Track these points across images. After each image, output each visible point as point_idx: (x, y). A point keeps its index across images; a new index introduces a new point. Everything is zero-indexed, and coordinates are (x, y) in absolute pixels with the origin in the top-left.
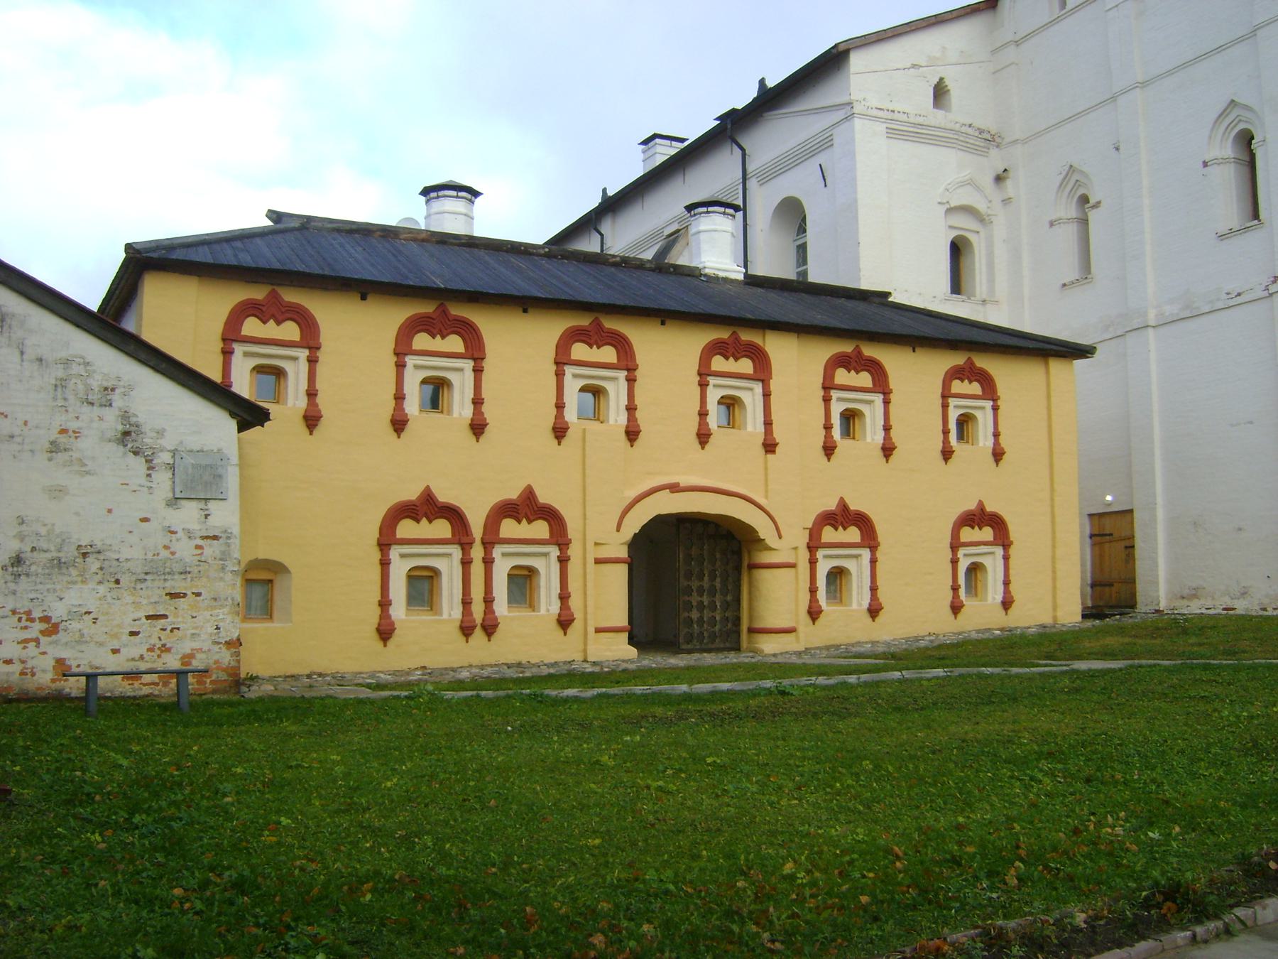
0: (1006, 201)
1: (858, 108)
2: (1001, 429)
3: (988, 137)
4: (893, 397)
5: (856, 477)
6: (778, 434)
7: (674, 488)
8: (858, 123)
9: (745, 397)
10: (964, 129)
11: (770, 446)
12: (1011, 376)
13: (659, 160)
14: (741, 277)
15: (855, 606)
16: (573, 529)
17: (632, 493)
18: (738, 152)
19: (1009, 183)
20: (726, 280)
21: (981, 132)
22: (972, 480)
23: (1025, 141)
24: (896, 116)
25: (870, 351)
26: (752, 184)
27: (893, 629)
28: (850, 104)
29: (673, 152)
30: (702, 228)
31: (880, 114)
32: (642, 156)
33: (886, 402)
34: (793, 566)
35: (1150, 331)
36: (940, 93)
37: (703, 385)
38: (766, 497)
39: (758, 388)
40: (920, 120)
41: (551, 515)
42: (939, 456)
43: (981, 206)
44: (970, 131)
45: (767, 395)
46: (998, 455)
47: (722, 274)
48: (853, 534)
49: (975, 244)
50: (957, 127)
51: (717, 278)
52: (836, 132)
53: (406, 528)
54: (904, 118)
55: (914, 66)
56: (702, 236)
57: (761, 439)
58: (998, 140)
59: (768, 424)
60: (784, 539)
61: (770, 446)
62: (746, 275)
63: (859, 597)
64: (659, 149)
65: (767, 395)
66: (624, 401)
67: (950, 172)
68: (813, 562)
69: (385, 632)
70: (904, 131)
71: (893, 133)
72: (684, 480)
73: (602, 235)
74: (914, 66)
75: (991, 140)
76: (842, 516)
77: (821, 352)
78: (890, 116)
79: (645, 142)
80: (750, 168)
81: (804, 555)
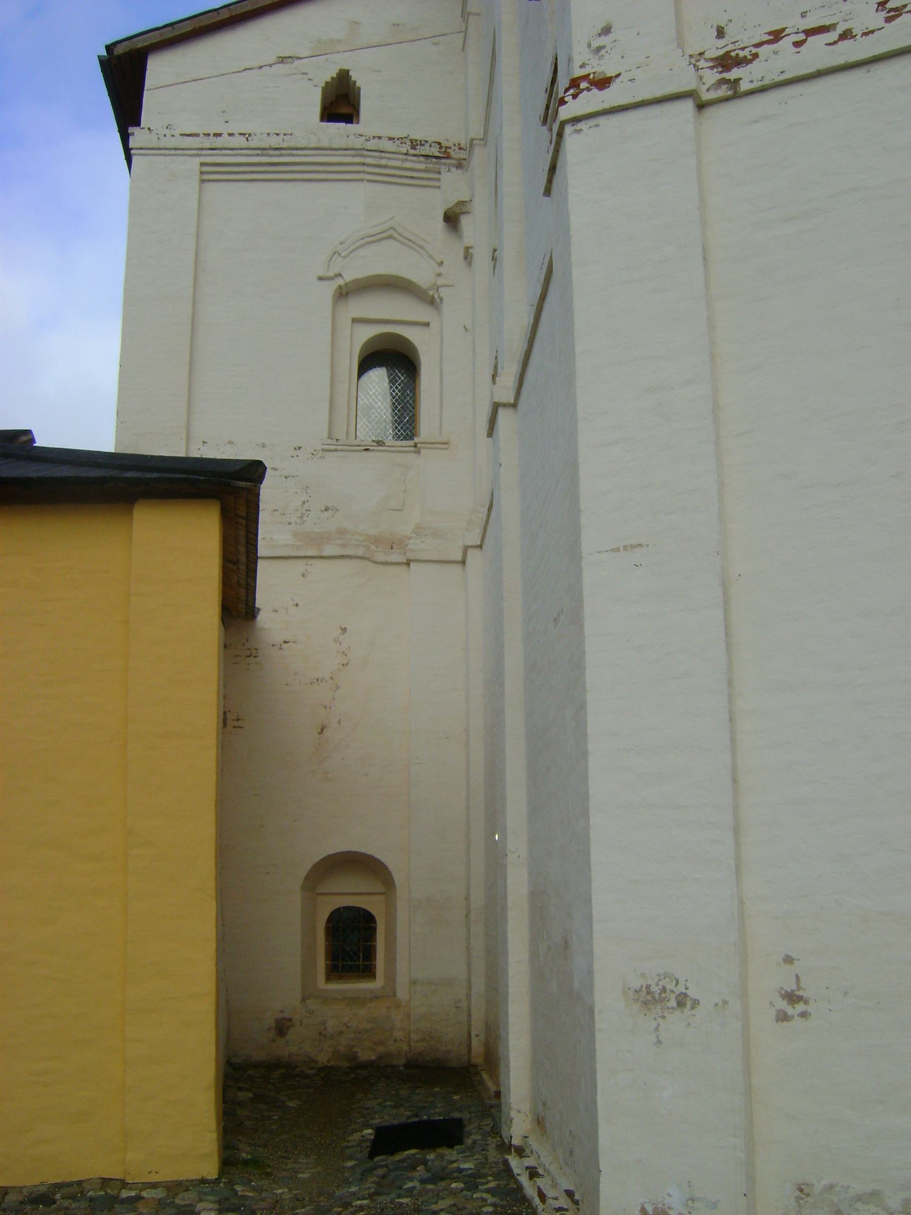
3: (435, 151)
19: (464, 221)
21: (414, 144)
36: (341, 103)
40: (275, 142)
43: (420, 273)
54: (240, 142)
55: (282, 60)
71: (209, 174)
74: (282, 60)
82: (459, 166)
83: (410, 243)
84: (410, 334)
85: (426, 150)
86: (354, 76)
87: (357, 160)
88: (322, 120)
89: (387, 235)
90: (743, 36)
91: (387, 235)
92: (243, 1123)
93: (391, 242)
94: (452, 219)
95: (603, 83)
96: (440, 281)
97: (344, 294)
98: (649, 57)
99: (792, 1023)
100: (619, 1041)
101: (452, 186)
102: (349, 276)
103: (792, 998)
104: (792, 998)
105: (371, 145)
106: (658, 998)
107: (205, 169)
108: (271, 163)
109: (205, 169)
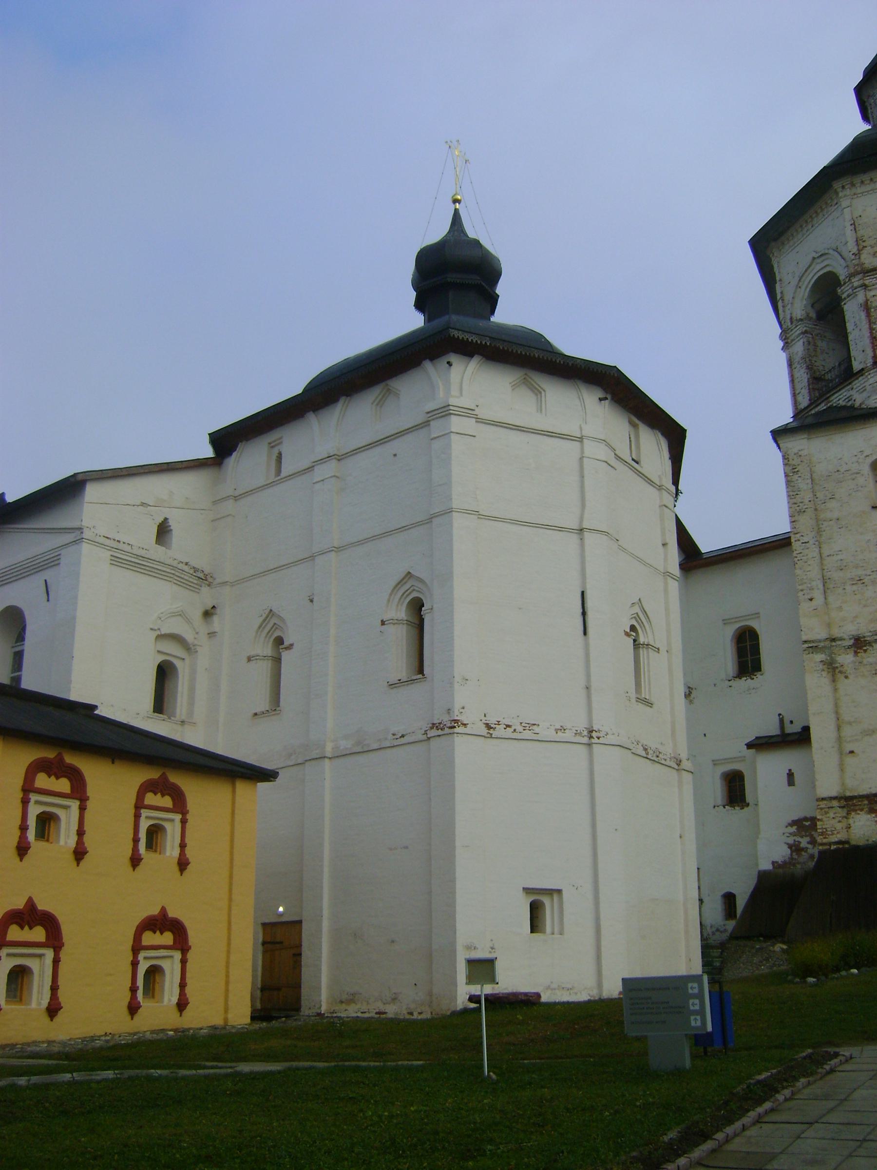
0: (212, 634)
1: (87, 534)
3: (201, 575)
4: (89, 804)
12: (201, 794)
15: (34, 1005)
16: (193, 937)
19: (216, 619)
21: (196, 570)
22: (156, 888)
24: (121, 546)
25: (70, 759)
31: (107, 542)
33: (82, 809)
41: (49, 922)
43: (189, 637)
44: (186, 568)
46: (183, 864)
48: (39, 934)
50: (175, 563)
55: (143, 504)
71: (116, 561)
74: (143, 504)
82: (209, 585)
83: (188, 621)
84: (176, 662)
87: (173, 572)
90: (492, 721)
91: (174, 615)
93: (179, 618)
96: (196, 642)
97: (161, 637)
98: (472, 717)
99: (645, 743)
101: (207, 597)
102: (164, 631)
103: (492, 948)
104: (492, 948)
105: (180, 566)
107: (556, 930)
108: (137, 564)
109: (556, 930)
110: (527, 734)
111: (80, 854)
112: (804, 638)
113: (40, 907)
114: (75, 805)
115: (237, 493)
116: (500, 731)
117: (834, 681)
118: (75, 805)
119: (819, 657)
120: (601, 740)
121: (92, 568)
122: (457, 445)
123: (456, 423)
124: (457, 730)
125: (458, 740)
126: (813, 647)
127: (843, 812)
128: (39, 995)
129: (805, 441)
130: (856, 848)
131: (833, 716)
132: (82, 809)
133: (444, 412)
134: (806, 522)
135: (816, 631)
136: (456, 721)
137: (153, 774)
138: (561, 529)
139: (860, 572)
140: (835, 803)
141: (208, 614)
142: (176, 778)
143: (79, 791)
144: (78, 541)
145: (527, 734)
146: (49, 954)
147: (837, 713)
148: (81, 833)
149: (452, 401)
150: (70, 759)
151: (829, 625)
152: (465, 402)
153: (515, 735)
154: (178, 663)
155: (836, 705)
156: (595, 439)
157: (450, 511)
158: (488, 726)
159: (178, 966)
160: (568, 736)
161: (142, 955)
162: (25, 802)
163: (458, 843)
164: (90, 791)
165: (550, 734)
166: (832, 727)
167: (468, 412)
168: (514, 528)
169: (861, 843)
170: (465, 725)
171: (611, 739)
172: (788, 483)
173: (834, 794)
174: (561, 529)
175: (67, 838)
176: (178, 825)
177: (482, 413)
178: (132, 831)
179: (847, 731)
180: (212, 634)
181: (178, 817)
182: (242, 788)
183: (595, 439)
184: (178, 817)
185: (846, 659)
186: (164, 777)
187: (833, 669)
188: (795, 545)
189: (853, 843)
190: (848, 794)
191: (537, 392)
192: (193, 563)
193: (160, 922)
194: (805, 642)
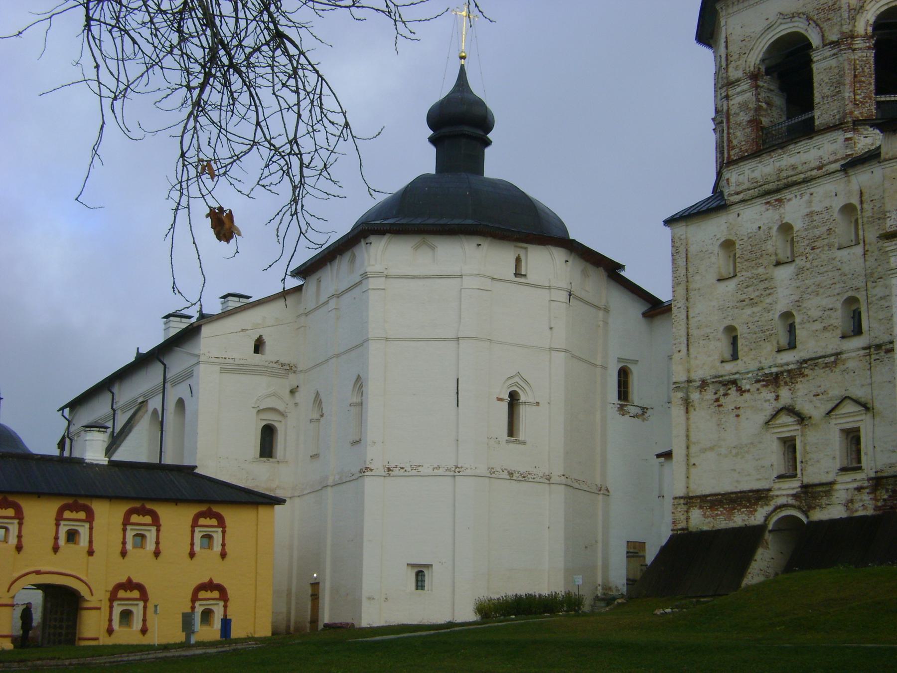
0: (296, 404)
1: (202, 359)
2: (226, 542)
3: (288, 368)
4: (162, 529)
5: (139, 566)
6: (95, 547)
7: (38, 573)
8: (202, 367)
9: (81, 530)
10: (271, 365)
11: (91, 553)
12: (235, 518)
13: (173, 332)
14: (106, 463)
15: (134, 628)
16: (230, 593)
17: (17, 575)
18: (110, 395)
19: (297, 394)
20: (97, 465)
21: (283, 365)
22: (208, 567)
23: (306, 371)
24: (227, 361)
25: (149, 506)
26: (168, 385)
27: (155, 638)
28: (198, 356)
29: (184, 326)
30: (88, 438)
31: (217, 360)
32: (163, 327)
33: (158, 531)
34: (99, 609)
35: (329, 488)
36: (259, 346)
37: (58, 525)
38: (87, 576)
39: (87, 525)
40: (242, 362)
41: (140, 588)
42: (187, 556)
43: (281, 408)
44: (275, 365)
45: (91, 529)
46: (223, 555)
47: (95, 462)
48: (136, 594)
49: (279, 429)
50: (266, 364)
51: (92, 464)
52: (195, 368)
53: (122, 594)
54: (231, 361)
55: (243, 330)
56: (87, 443)
57: (87, 549)
58: (294, 369)
59: (91, 542)
60: (96, 594)
61: (91, 553)
62: (109, 462)
63: (137, 624)
64: (172, 324)
65: (91, 529)
66: (16, 533)
67: (263, 388)
68: (111, 607)
69: (110, 631)
70: (230, 368)
71: (223, 370)
72: (43, 569)
73: (113, 394)
74: (243, 330)
75: (289, 369)
76: (129, 585)
77: (121, 509)
78: (223, 361)
79: (167, 317)
80: (168, 376)
81: (105, 605)
82: (294, 372)
85: (285, 367)
86: (264, 337)
88: (417, 589)
89: (269, 396)
90: (392, 465)
91: (269, 396)
92: (786, 228)
94: (292, 392)
95: (372, 470)
98: (378, 466)
100: (365, 604)
106: (370, 598)
108: (241, 369)
110: (414, 472)
111: (157, 553)
112: (674, 380)
113: (134, 581)
114: (154, 529)
115: (307, 311)
116: (396, 472)
117: (687, 413)
118: (154, 529)
119: (680, 395)
120: (461, 474)
121: (208, 379)
122: (373, 296)
123: (372, 283)
124: (366, 473)
125: (367, 479)
126: (677, 387)
127: (685, 508)
128: (137, 624)
129: (684, 228)
130: (691, 532)
131: (684, 438)
132: (158, 531)
133: (365, 276)
134: (681, 290)
135: (681, 377)
136: (367, 468)
137: (203, 508)
138: (445, 340)
139: (708, 330)
140: (682, 501)
141: (292, 392)
142: (216, 509)
143: (156, 522)
144: (198, 363)
145: (414, 472)
146: (141, 604)
147: (687, 436)
148: (157, 543)
149: (368, 269)
150: (149, 506)
151: (689, 371)
152: (378, 268)
153: (406, 474)
154: (276, 424)
155: (688, 430)
156: (471, 275)
157: (367, 340)
158: (389, 470)
159: (222, 609)
160: (441, 472)
161: (197, 604)
162: (124, 530)
163: (365, 539)
164: (162, 521)
165: (429, 471)
166: (684, 447)
167: (379, 275)
168: (412, 344)
169: (694, 530)
170: (372, 470)
171: (469, 472)
172: (673, 260)
173: (681, 494)
174: (445, 340)
175: (150, 546)
176: (220, 534)
177: (393, 271)
178: (190, 539)
179: (693, 449)
180: (296, 404)
181: (220, 530)
182: (263, 511)
183: (471, 275)
184: (220, 530)
185: (695, 396)
186: (210, 509)
187: (687, 404)
188: (674, 309)
189: (690, 529)
190: (691, 495)
191: (433, 248)
192: (282, 361)
193: (210, 586)
194: (674, 383)
